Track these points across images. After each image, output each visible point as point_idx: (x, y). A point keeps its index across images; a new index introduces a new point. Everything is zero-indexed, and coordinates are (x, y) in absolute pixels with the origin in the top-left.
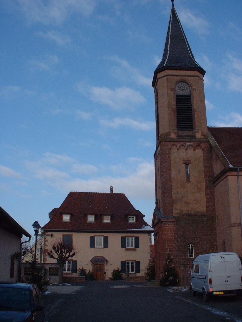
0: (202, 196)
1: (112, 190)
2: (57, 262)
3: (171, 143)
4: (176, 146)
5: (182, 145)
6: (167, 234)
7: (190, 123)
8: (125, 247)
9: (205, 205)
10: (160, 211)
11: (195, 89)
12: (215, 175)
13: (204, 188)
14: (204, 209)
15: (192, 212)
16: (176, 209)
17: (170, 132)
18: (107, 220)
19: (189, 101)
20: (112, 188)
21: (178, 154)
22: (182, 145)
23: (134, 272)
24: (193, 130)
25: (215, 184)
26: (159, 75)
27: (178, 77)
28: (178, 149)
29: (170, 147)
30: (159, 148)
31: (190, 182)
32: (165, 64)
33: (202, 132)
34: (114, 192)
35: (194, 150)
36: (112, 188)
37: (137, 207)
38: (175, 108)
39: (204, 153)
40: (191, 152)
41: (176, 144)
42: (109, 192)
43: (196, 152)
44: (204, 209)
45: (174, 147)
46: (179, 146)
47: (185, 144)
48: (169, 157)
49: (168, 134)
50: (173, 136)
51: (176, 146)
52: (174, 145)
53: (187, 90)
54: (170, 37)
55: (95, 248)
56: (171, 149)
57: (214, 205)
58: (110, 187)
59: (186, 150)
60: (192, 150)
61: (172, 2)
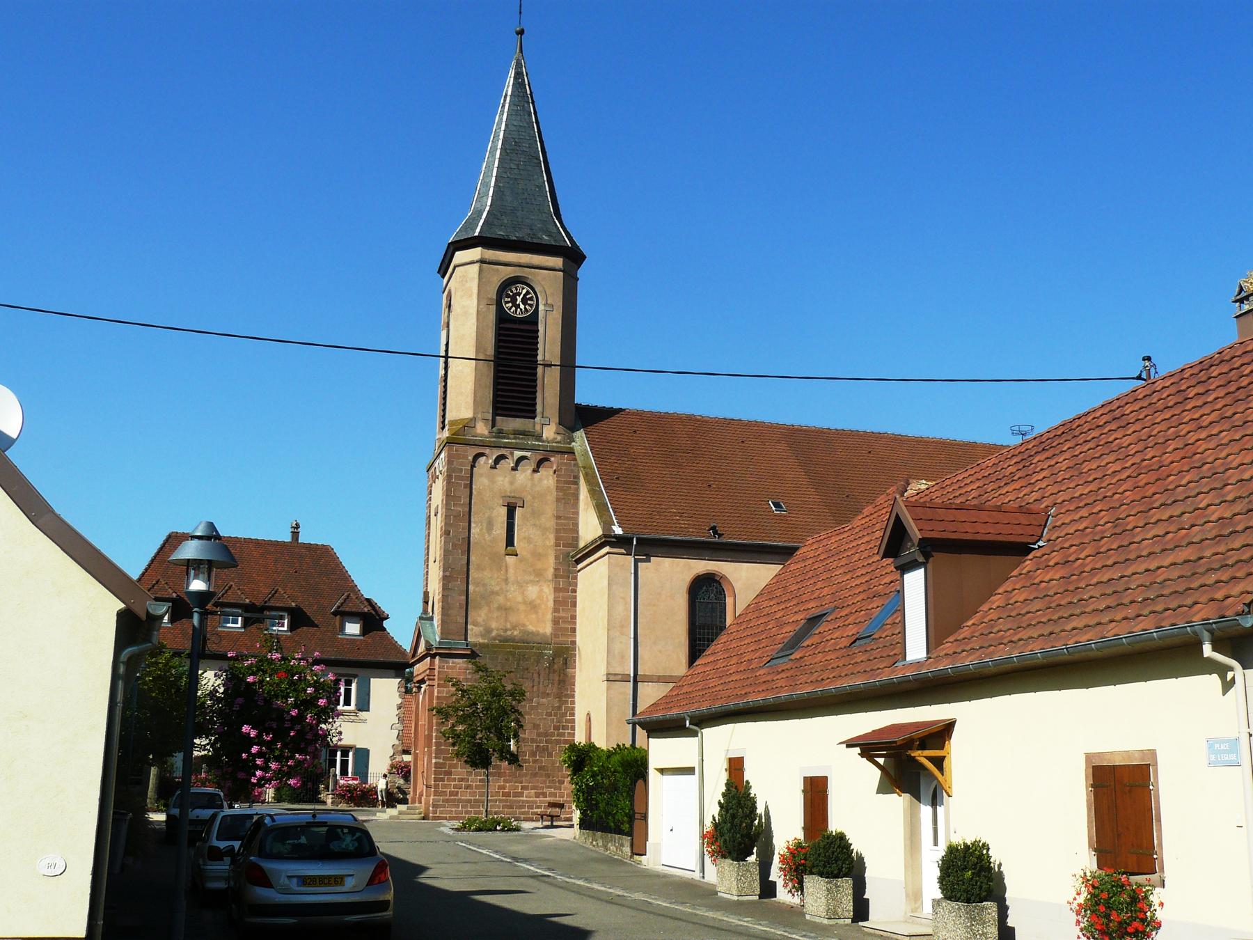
0: (544, 593)
1: (295, 535)
2: (471, 296)
7: (503, 378)
10: (432, 625)
12: (582, 545)
13: (550, 573)
14: (547, 629)
16: (476, 624)
17: (474, 419)
19: (504, 341)
23: (352, 707)
25: (579, 567)
26: (460, 256)
30: (442, 455)
32: (478, 230)
37: (368, 590)
41: (487, 451)
42: (287, 538)
44: (547, 629)
47: (512, 454)
49: (468, 425)
50: (482, 429)
54: (499, 146)
57: (574, 617)
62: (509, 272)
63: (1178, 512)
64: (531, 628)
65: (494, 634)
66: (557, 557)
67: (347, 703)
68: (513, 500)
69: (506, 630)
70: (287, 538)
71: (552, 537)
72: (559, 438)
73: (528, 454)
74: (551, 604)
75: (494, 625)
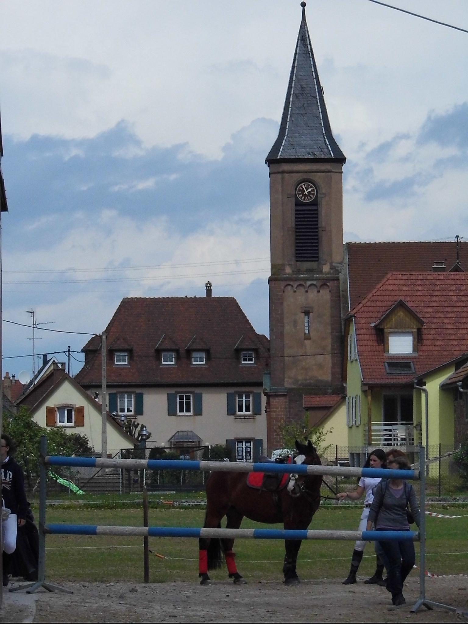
1: (209, 291)
3: (285, 283)
4: (292, 286)
5: (300, 285)
6: (275, 412)
8: (234, 414)
9: (330, 371)
11: (324, 194)
13: (329, 348)
15: (312, 381)
17: (283, 265)
18: (199, 361)
20: (209, 286)
21: (296, 298)
22: (300, 285)
23: (191, 413)
24: (318, 261)
27: (299, 174)
28: (295, 292)
29: (282, 287)
31: (310, 339)
33: (331, 264)
34: (215, 294)
35: (319, 292)
36: (209, 286)
38: (293, 225)
39: (332, 296)
40: (313, 295)
41: (292, 283)
42: (204, 295)
43: (320, 294)
45: (290, 287)
46: (295, 286)
47: (306, 283)
48: (282, 304)
50: (288, 270)
51: (292, 286)
52: (289, 285)
53: (313, 194)
55: (178, 416)
56: (284, 292)
58: (207, 284)
59: (307, 292)
60: (316, 292)
61: (302, 8)
62: (300, 176)
63: (431, 347)
64: (320, 378)
65: (300, 382)
66: (332, 339)
67: (188, 410)
68: (308, 309)
69: (306, 380)
70: (204, 295)
71: (329, 327)
72: (332, 271)
73: (314, 282)
74: (330, 365)
75: (300, 378)
